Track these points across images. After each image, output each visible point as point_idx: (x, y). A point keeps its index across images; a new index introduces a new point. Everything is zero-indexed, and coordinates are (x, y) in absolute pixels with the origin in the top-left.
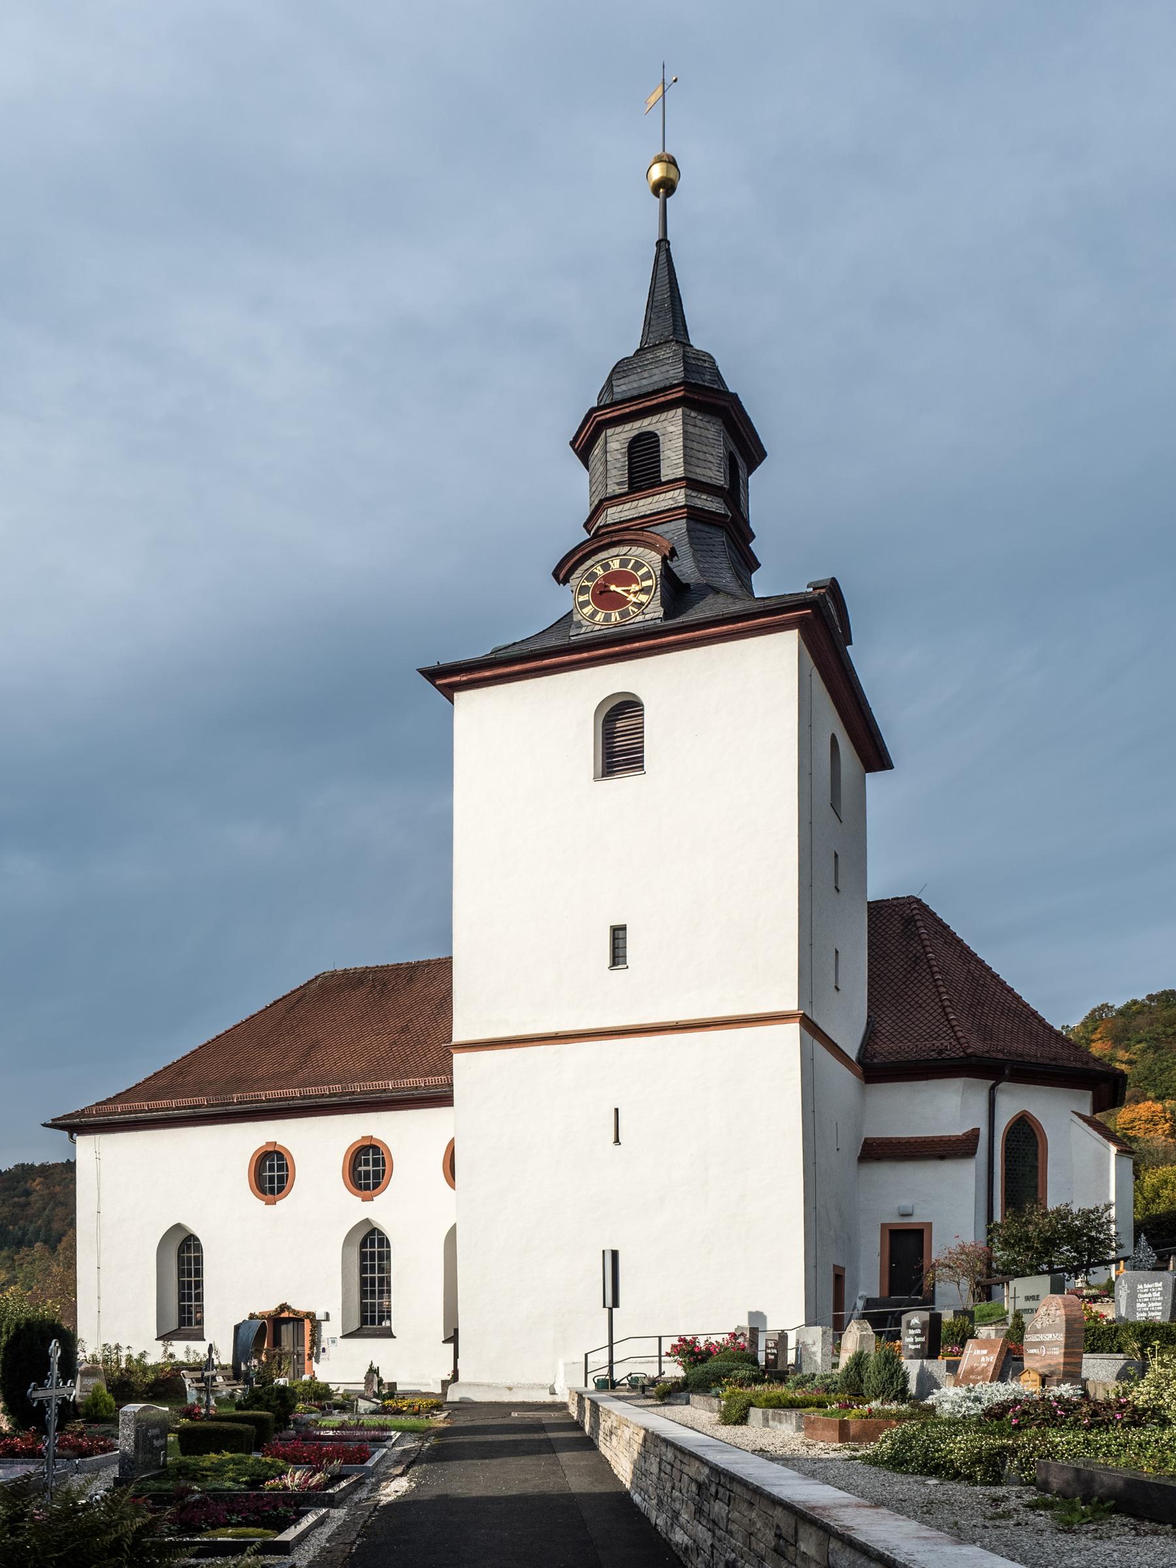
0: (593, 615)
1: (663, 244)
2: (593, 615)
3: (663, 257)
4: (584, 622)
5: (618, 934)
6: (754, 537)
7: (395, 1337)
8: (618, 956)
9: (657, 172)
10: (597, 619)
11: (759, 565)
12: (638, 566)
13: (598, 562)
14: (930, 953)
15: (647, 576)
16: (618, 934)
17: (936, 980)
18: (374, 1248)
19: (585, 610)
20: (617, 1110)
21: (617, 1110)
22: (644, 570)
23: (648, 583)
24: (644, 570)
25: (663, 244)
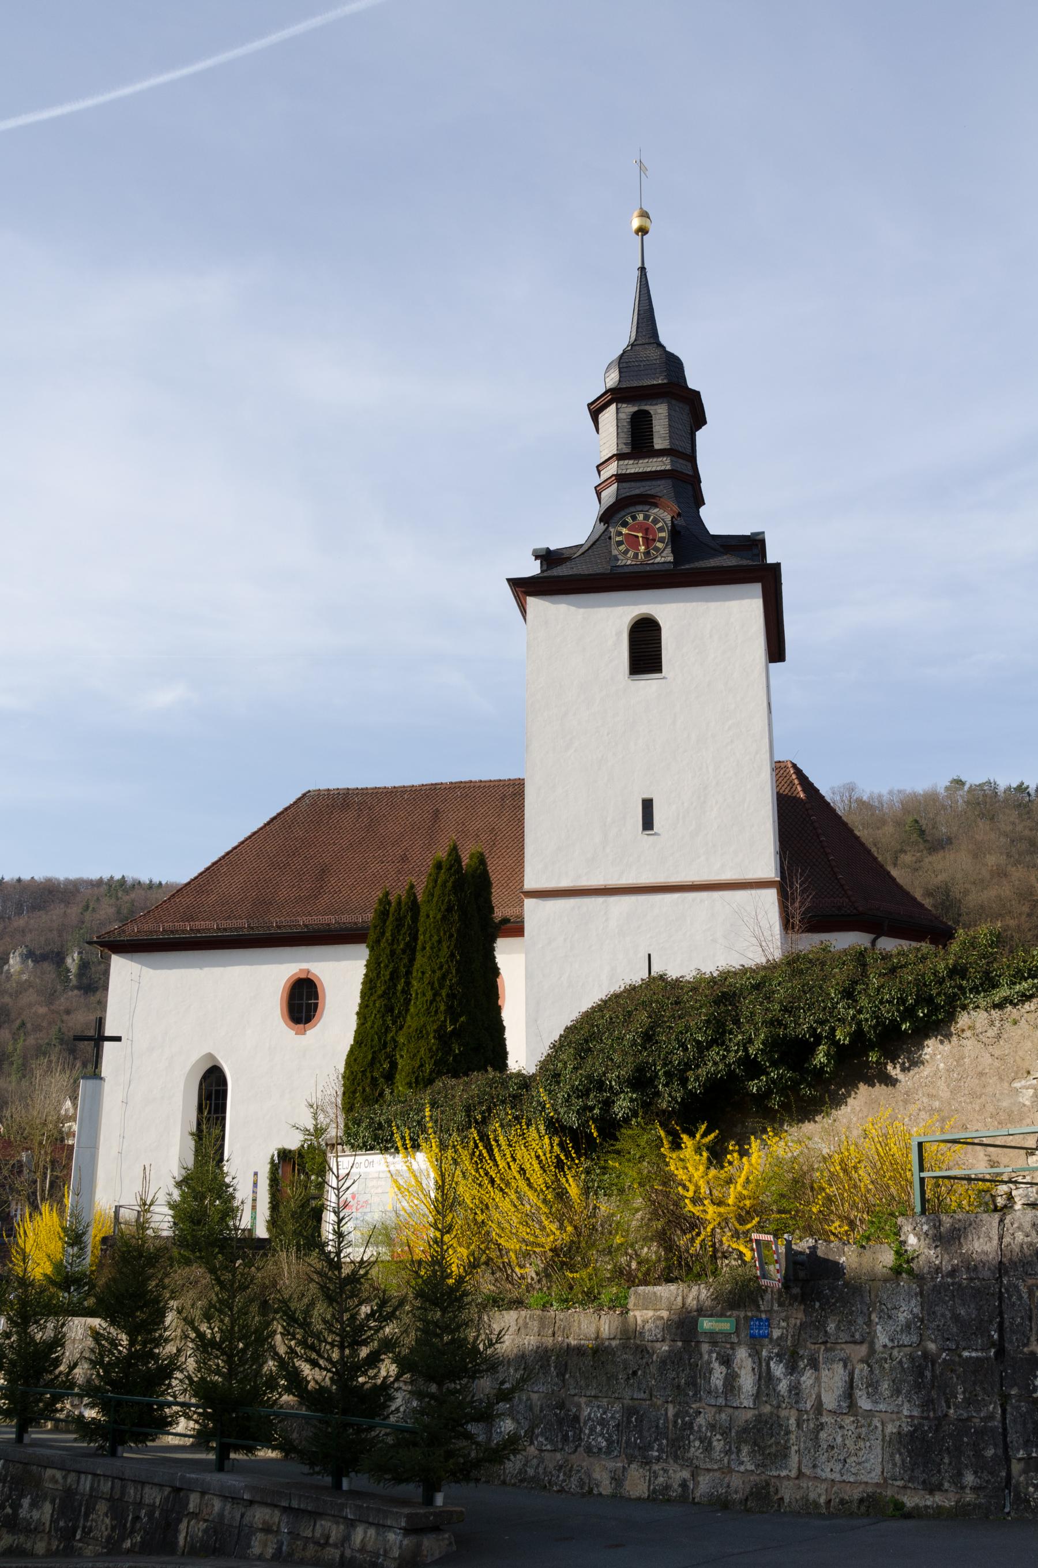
0: (626, 552)
1: (643, 269)
2: (626, 552)
3: (643, 280)
4: (620, 557)
5: (648, 806)
6: (704, 504)
7: (509, 580)
8: (648, 823)
9: (636, 223)
10: (629, 555)
11: (704, 504)
12: (655, 521)
13: (629, 514)
14: (812, 815)
15: (661, 529)
16: (648, 806)
17: (821, 842)
18: (302, 999)
19: (620, 548)
20: (649, 955)
21: (649, 955)
22: (660, 525)
23: (663, 534)
24: (660, 525)
25: (643, 269)
